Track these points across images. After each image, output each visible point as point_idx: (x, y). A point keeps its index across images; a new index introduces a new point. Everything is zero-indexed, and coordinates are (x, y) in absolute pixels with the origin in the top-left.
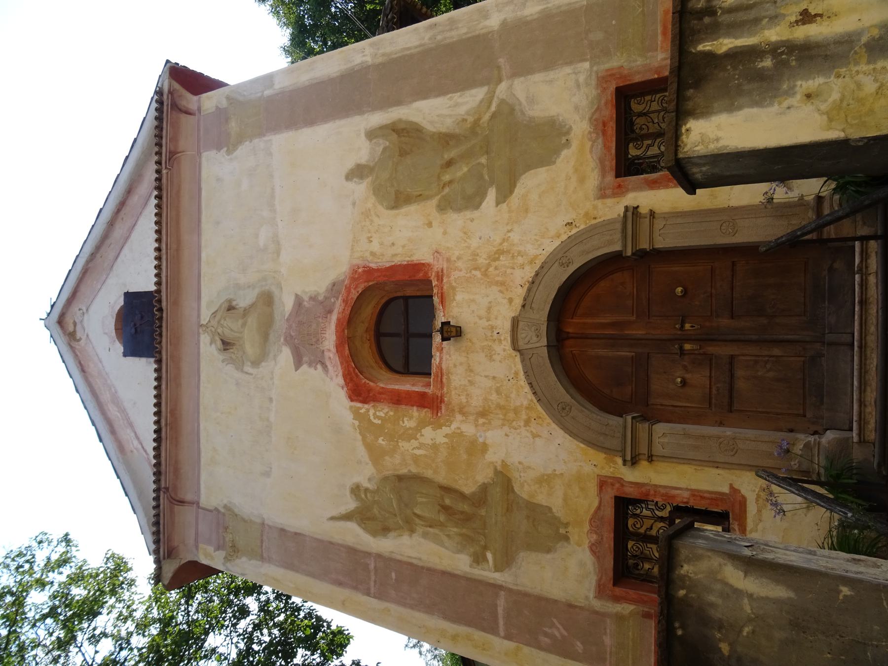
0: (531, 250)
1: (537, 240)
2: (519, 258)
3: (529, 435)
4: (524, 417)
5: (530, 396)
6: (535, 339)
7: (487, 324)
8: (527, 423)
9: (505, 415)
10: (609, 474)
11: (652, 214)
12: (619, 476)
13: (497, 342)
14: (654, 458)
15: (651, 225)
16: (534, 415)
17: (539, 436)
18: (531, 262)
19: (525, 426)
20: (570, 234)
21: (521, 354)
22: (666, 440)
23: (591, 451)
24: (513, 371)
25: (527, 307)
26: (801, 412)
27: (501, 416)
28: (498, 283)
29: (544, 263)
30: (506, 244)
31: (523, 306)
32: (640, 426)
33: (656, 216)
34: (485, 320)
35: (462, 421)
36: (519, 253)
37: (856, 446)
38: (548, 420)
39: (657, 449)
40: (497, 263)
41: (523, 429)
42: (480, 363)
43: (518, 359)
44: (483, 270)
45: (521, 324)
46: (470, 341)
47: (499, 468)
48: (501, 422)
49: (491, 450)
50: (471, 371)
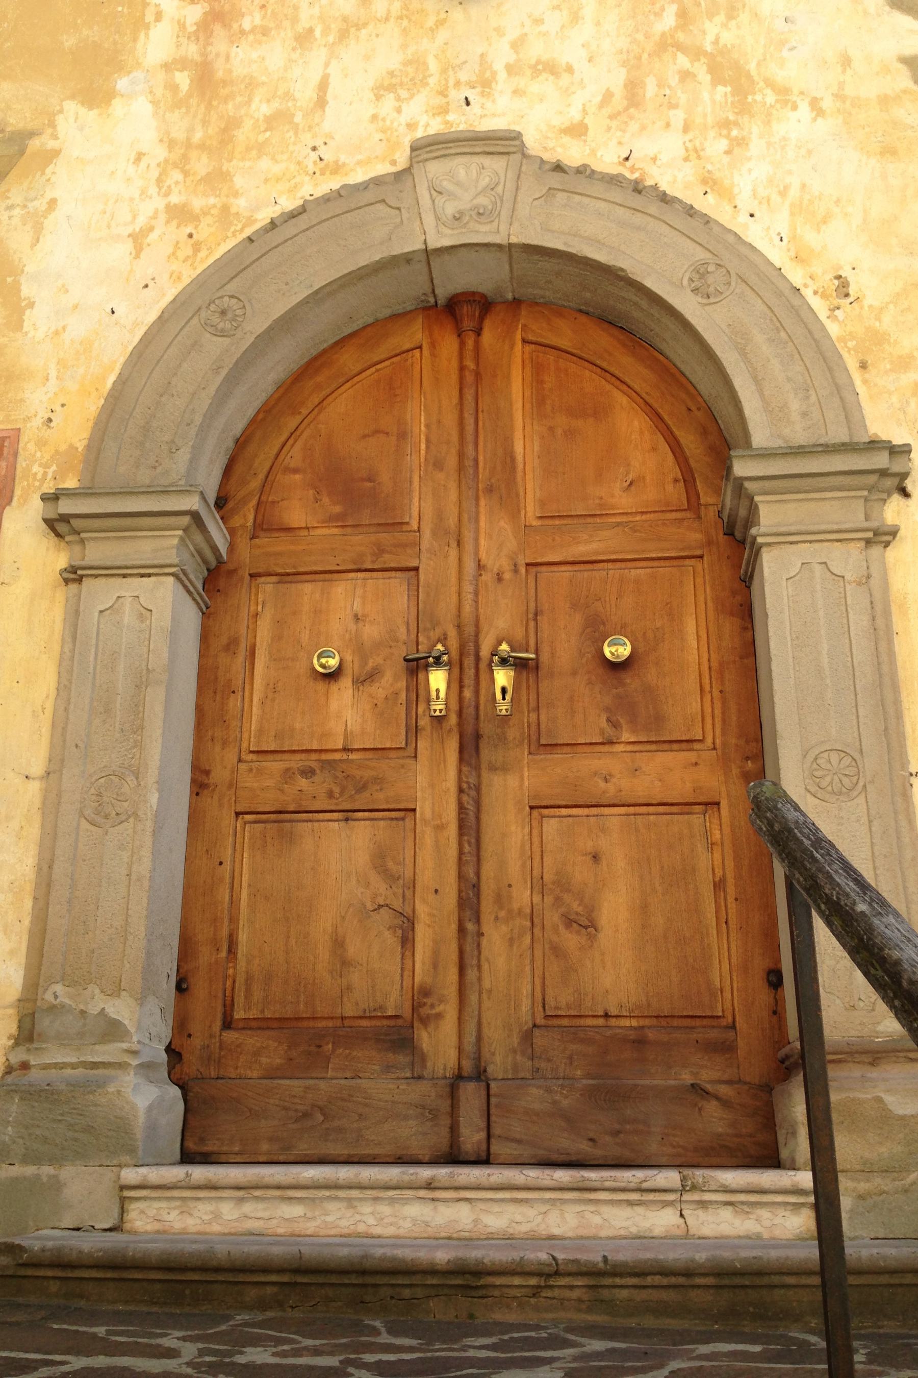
0: (748, 180)
1: (783, 193)
2: (723, 144)
3: (141, 221)
4: (197, 203)
5: (264, 216)
6: (450, 209)
7: (499, 67)
8: (179, 214)
9: (202, 147)
10: (21, 464)
11: (883, 536)
12: (18, 492)
13: (439, 100)
14: (73, 587)
15: (840, 536)
16: (204, 231)
17: (138, 251)
18: (709, 183)
19: (169, 208)
20: (808, 293)
21: (398, 176)
22: (128, 616)
23: (94, 406)
24: (343, 158)
25: (555, 180)
26: (239, 1014)
27: (198, 135)
28: (633, 90)
29: (707, 220)
30: (771, 98)
31: (558, 168)
32: (173, 539)
33: (876, 551)
34: (512, 58)
35: (182, 25)
36: (742, 142)
37: (109, 1174)
38: (188, 275)
39: (100, 593)
40: (704, 77)
41: (159, 203)
42: (367, 58)
43: (383, 169)
44: (681, 36)
45: (497, 164)
46: (441, 23)
47: (35, 144)
48: (179, 134)
49: (90, 116)
50: (343, 35)
